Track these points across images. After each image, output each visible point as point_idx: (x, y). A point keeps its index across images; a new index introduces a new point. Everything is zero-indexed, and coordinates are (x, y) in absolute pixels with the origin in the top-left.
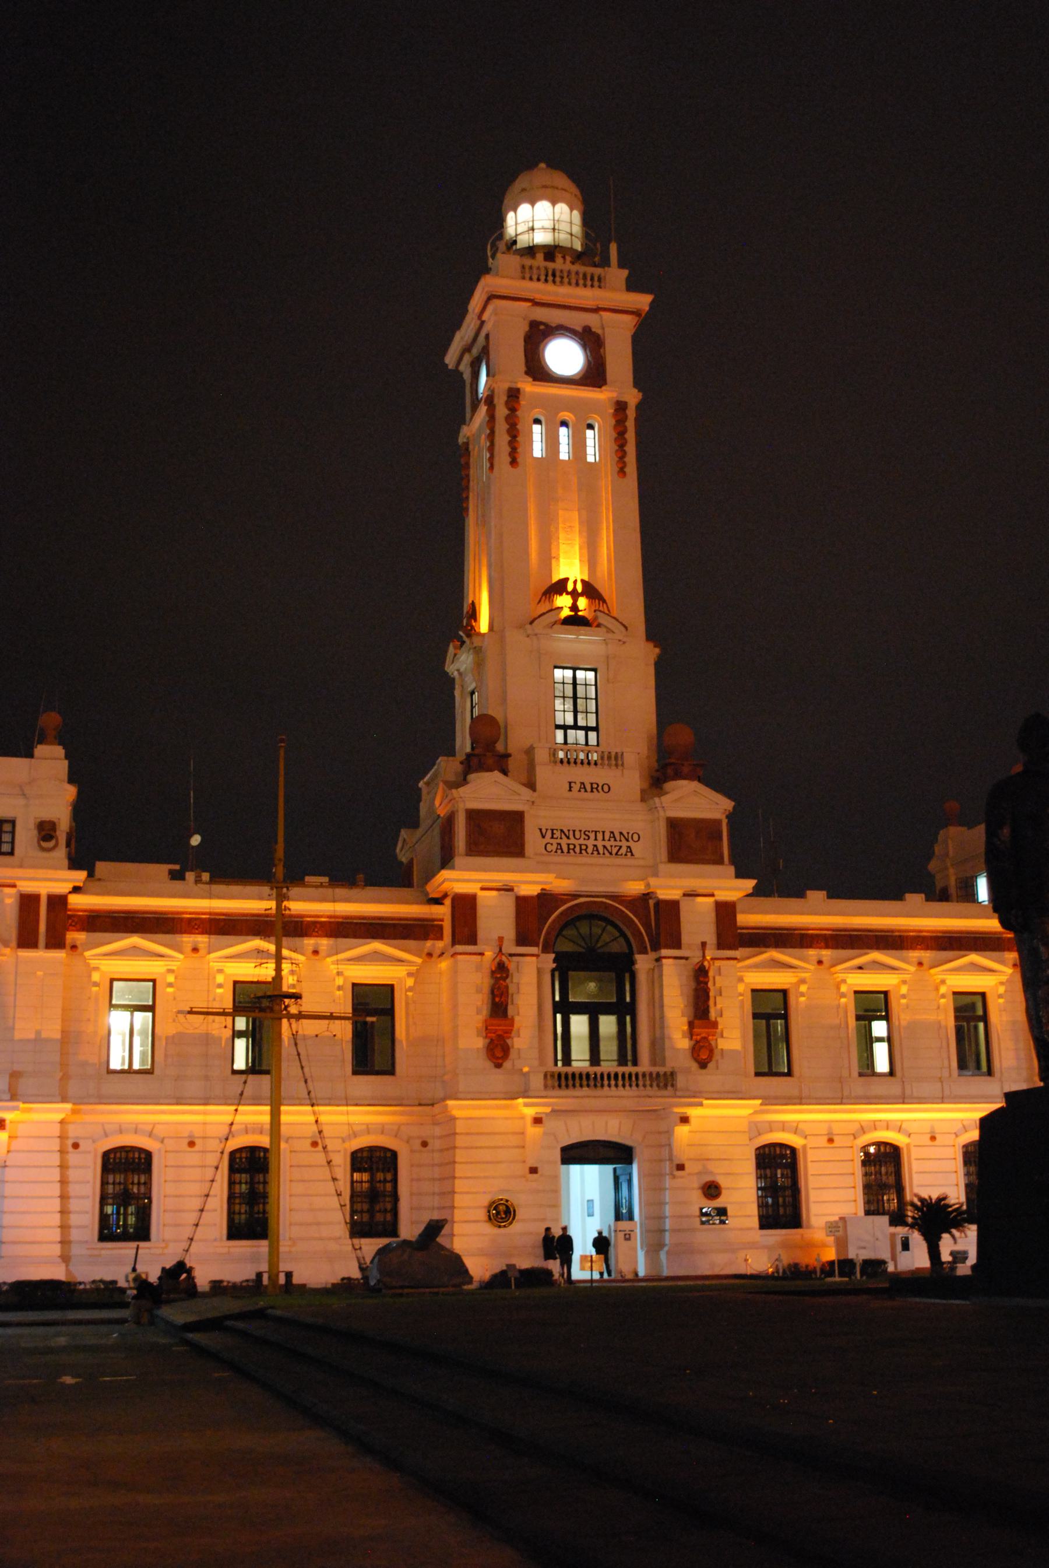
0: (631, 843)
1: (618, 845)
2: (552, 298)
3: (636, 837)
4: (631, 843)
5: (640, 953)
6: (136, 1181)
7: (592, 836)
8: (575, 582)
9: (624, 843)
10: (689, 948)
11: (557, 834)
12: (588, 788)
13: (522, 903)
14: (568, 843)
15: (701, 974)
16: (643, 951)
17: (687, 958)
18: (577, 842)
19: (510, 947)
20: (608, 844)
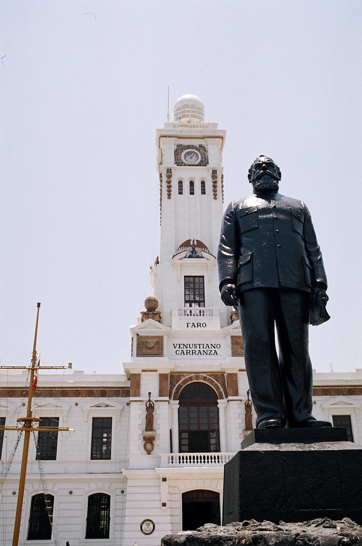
0: (216, 349)
1: (211, 349)
2: (193, 134)
3: (218, 346)
4: (216, 349)
5: (220, 399)
6: (39, 513)
7: (198, 346)
8: (193, 241)
9: (213, 349)
10: (144, 397)
11: (182, 346)
12: (196, 325)
13: (163, 377)
14: (186, 350)
15: (150, 408)
16: (222, 398)
17: (241, 400)
18: (191, 350)
19: (155, 397)
20: (205, 350)
